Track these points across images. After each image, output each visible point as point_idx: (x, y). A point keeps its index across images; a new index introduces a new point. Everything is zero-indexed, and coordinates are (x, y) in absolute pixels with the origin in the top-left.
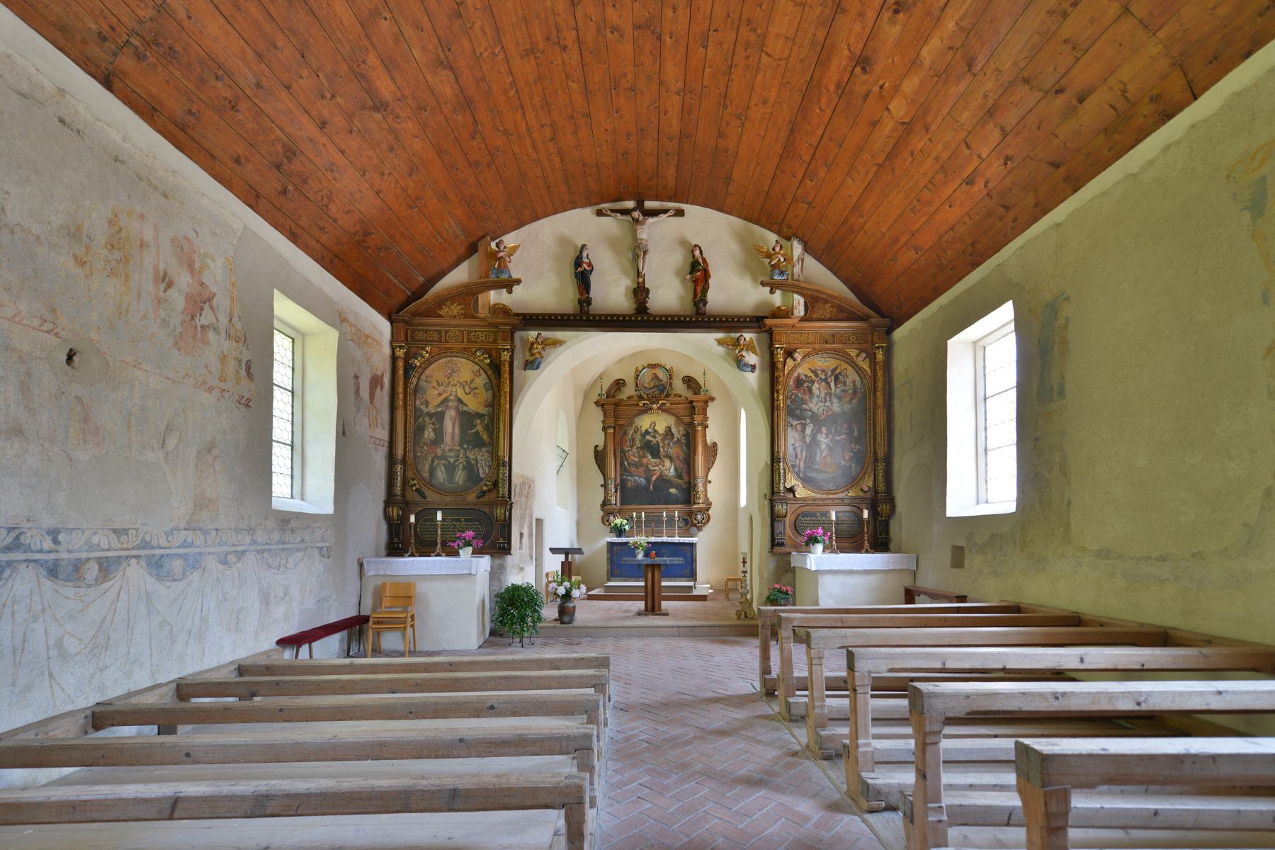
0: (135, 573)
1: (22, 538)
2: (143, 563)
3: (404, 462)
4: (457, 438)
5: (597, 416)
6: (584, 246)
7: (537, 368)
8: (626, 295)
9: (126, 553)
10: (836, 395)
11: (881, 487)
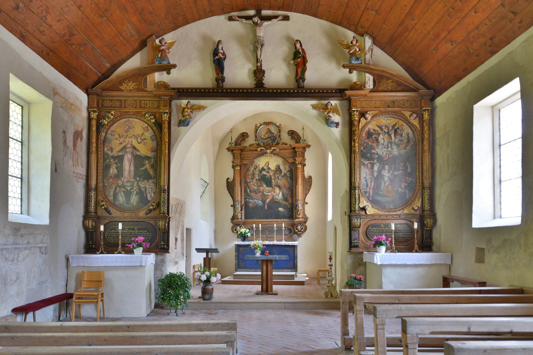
3: (96, 189)
4: (132, 173)
5: (228, 158)
6: (219, 42)
7: (187, 125)
8: (249, 75)
10: (395, 143)
11: (427, 207)
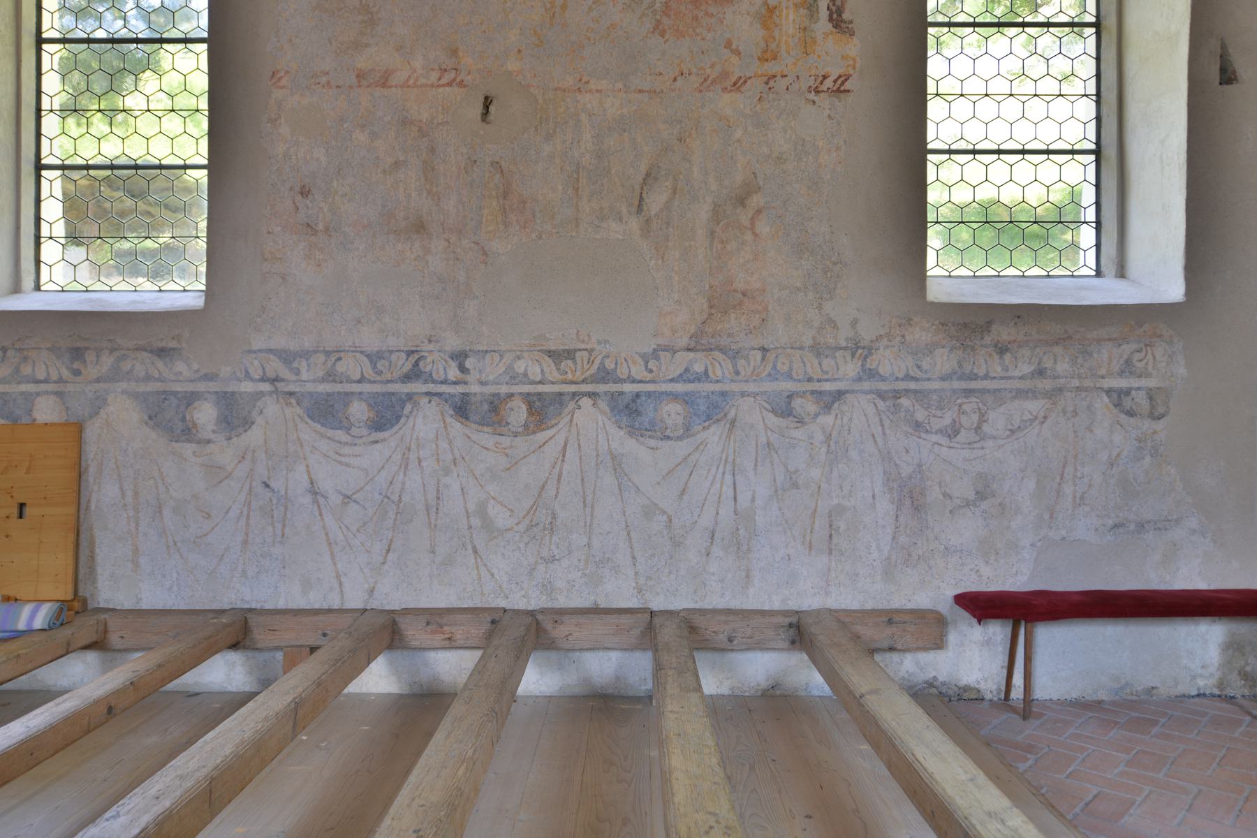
0: (590, 422)
1: (421, 364)
2: (603, 404)
9: (573, 388)
